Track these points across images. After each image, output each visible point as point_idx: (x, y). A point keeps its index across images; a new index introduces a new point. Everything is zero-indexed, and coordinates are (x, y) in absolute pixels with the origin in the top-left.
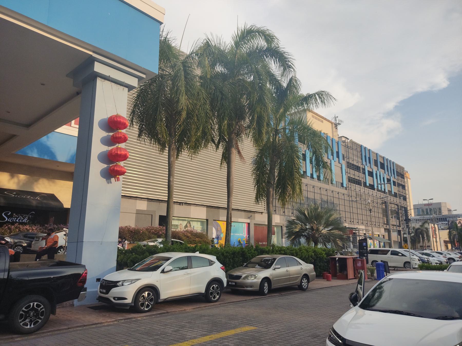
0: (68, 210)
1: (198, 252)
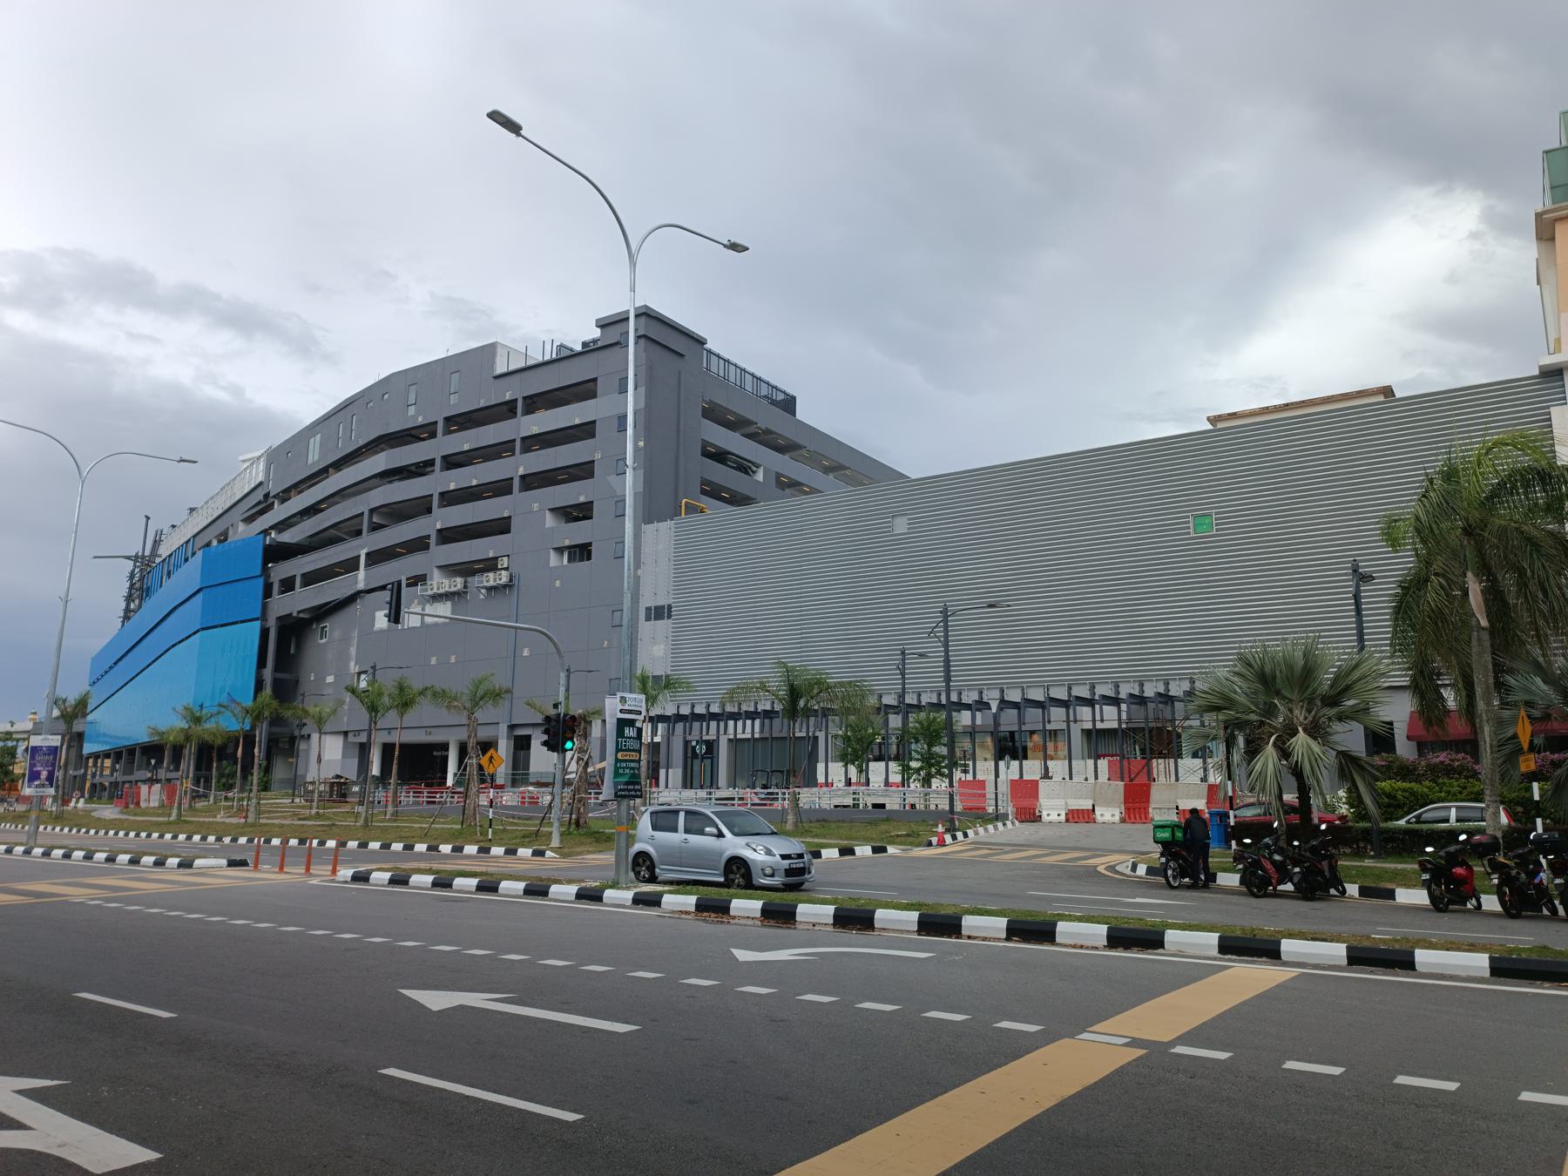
0: (1348, 948)
1: (1555, 412)
